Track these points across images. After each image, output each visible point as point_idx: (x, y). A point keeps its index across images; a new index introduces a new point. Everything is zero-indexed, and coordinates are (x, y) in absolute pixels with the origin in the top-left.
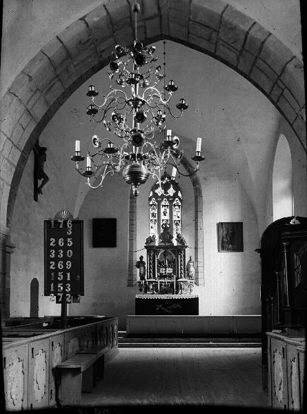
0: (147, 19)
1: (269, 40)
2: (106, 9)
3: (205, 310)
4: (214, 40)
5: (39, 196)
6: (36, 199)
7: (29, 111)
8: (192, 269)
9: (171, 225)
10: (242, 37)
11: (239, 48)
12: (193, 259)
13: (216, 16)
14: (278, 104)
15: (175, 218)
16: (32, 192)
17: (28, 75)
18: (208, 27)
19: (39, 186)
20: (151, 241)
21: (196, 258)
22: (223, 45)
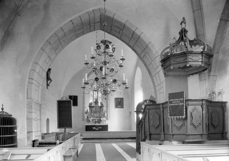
0: (95, 23)
1: (142, 35)
2: (80, 18)
3: (110, 129)
4: (121, 33)
5: (48, 87)
6: (47, 88)
7: (49, 57)
8: (106, 114)
9: (98, 98)
10: (132, 33)
11: (130, 37)
12: (106, 111)
13: (222, 16)
14: (144, 59)
15: (99, 96)
16: (46, 85)
17: (49, 43)
18: (119, 28)
19: (48, 84)
20: (91, 104)
21: (107, 110)
22: (124, 35)
